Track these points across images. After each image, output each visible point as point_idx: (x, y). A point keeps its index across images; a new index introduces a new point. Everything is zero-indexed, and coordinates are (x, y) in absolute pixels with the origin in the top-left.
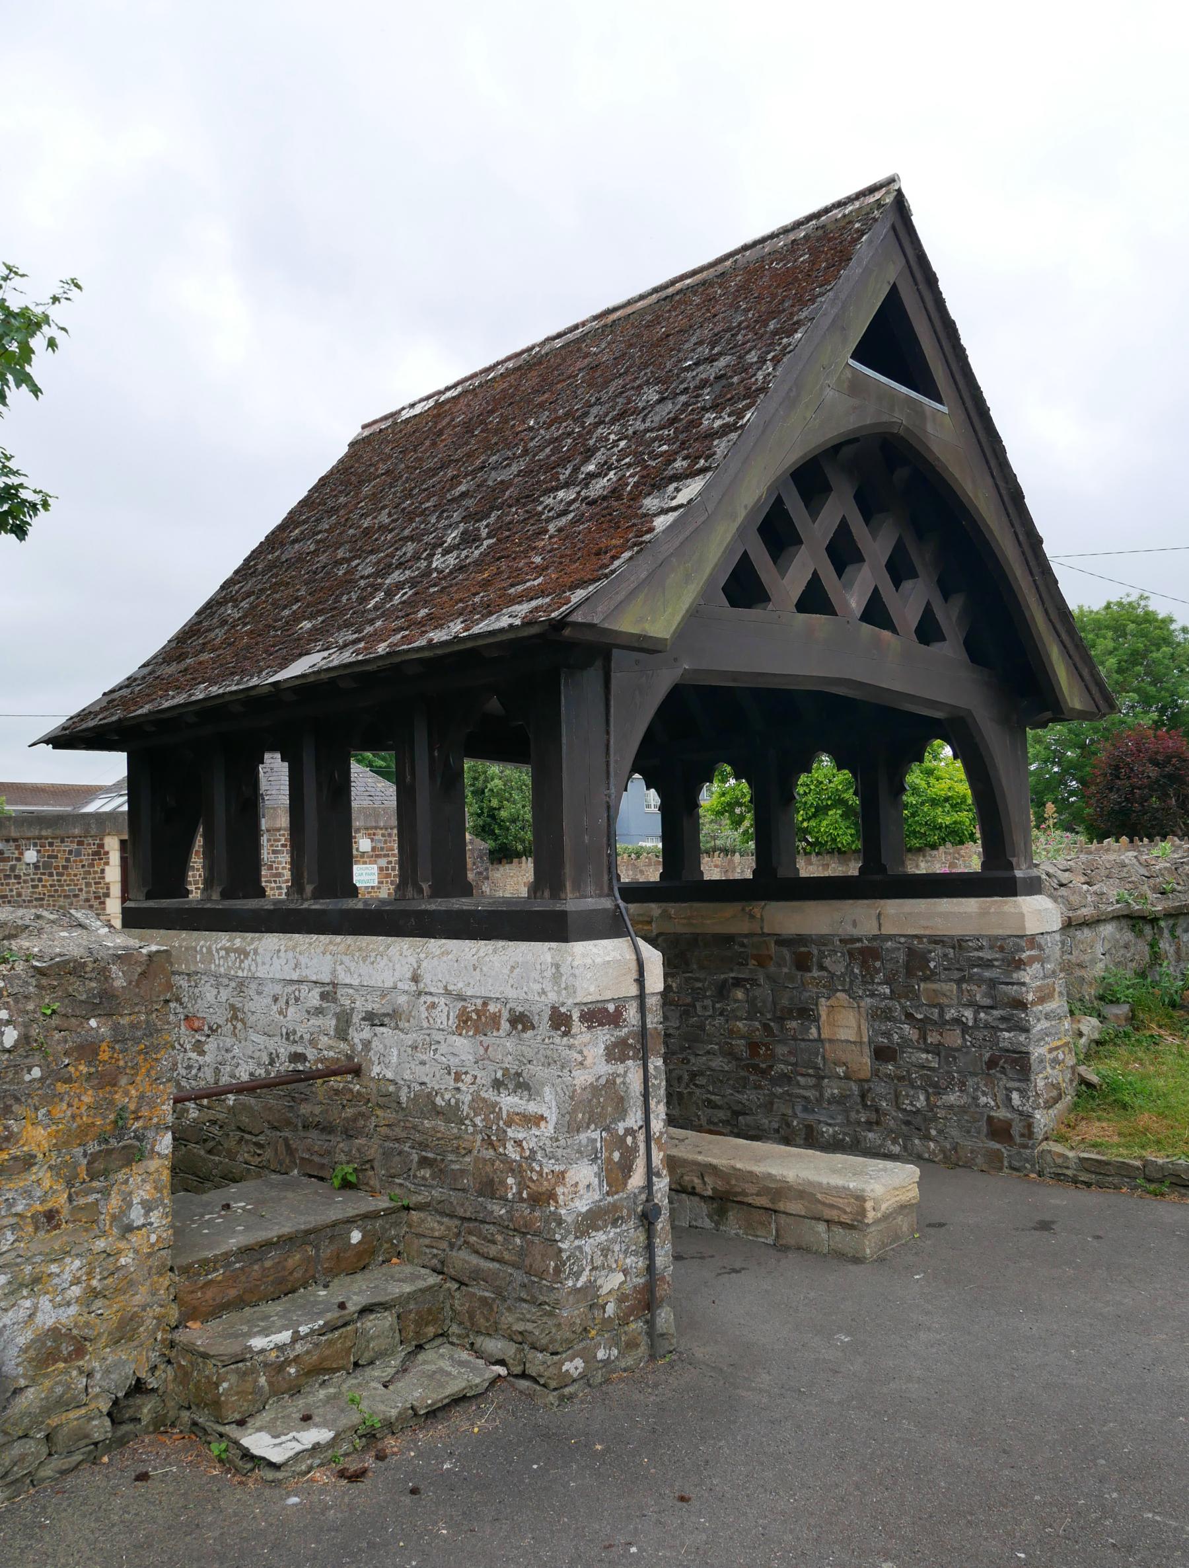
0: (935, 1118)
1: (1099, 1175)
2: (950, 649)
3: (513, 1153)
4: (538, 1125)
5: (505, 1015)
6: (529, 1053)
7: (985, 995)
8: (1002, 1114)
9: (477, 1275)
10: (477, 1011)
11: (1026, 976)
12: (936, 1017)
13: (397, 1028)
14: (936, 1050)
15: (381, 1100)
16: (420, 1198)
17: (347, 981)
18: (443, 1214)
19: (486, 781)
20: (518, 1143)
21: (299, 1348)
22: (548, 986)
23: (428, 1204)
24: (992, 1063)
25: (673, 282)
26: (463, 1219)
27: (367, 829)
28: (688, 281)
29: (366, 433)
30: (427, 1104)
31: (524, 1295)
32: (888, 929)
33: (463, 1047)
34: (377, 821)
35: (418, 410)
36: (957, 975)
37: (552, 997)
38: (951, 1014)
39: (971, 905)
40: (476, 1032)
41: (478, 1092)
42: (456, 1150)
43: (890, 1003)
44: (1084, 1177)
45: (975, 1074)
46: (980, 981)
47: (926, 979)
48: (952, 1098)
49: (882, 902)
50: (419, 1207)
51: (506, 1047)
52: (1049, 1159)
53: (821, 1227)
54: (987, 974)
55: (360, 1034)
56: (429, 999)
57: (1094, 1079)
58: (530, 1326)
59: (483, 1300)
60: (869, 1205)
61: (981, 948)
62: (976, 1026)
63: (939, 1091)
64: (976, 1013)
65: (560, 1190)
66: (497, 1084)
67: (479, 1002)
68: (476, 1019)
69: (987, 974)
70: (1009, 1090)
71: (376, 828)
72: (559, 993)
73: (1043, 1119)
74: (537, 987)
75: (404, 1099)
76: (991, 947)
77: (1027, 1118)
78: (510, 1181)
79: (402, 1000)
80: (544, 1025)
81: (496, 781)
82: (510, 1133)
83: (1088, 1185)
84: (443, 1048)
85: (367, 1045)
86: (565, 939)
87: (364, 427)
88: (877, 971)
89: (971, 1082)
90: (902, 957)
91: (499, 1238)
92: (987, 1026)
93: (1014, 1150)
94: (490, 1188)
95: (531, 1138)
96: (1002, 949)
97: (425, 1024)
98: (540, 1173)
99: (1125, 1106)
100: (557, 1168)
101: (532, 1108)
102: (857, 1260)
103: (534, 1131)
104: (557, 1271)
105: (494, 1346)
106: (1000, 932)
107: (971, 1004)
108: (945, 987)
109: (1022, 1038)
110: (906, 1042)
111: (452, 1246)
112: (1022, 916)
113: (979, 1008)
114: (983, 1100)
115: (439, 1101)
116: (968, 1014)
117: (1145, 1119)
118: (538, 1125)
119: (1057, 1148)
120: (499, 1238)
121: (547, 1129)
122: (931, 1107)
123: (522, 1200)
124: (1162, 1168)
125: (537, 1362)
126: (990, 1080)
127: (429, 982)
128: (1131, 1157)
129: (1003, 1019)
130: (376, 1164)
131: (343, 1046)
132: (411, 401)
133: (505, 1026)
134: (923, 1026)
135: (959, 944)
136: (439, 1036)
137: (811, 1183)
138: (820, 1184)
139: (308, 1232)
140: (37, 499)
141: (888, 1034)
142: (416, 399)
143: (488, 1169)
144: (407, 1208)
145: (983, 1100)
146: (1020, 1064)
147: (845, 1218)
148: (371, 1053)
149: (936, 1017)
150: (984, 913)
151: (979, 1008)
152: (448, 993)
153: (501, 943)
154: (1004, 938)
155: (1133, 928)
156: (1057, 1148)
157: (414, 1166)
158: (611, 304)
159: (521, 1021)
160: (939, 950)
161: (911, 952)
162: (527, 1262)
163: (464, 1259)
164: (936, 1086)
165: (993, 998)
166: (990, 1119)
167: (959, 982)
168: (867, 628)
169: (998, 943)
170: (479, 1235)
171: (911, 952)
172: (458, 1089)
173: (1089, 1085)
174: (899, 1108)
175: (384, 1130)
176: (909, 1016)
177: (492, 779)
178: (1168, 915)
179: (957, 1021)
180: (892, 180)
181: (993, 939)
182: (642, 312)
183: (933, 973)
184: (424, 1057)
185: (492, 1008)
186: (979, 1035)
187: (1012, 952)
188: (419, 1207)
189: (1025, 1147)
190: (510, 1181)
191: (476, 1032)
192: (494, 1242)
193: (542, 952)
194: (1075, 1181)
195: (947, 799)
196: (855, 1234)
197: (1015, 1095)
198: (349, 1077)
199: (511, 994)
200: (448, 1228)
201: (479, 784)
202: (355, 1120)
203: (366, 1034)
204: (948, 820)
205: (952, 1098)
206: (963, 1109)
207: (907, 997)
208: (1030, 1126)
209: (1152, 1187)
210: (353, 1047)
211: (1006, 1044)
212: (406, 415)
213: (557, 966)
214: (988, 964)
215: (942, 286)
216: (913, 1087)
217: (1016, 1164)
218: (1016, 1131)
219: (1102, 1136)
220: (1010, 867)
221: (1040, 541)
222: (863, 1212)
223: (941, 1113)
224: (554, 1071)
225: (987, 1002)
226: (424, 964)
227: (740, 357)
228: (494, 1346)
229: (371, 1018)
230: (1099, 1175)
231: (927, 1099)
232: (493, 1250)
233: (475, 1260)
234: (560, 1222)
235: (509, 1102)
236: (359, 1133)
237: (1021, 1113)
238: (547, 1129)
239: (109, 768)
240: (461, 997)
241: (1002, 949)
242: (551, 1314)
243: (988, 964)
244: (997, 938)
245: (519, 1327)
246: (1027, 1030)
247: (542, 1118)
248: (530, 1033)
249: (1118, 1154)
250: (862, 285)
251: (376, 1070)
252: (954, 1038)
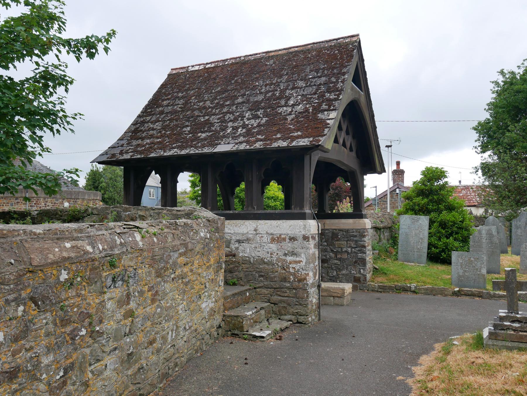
0: (339, 278)
1: (383, 289)
2: (354, 154)
3: (291, 270)
4: (300, 263)
5: (287, 237)
6: (296, 246)
7: (354, 244)
8: (358, 275)
9: (281, 301)
10: (278, 238)
11: (366, 239)
12: (340, 251)
13: (248, 243)
14: (340, 259)
15: (243, 262)
16: (260, 285)
17: (229, 232)
18: (267, 288)
19: (99, 183)
20: (294, 268)
21: (253, 316)
22: (301, 230)
23: (262, 286)
24: (356, 262)
25: (291, 48)
26: (275, 288)
27: (67, 199)
28: (296, 49)
29: (174, 72)
30: (262, 261)
31: (297, 303)
32: (326, 227)
33: (274, 247)
34: (71, 196)
35: (197, 68)
36: (346, 239)
37: (303, 233)
38: (344, 250)
39: (351, 221)
40: (278, 242)
41: (279, 257)
42: (272, 272)
43: (327, 247)
44: (380, 290)
45: (350, 265)
46: (353, 241)
47: (337, 240)
48: (344, 272)
49: (325, 220)
50: (259, 287)
51: (288, 246)
52: (370, 286)
53: (332, 298)
54: (355, 239)
55: (233, 246)
56: (260, 235)
57: (377, 267)
58: (299, 311)
59: (284, 307)
60: (345, 291)
61: (353, 232)
62: (351, 252)
63: (340, 270)
64: (352, 249)
65: (307, 277)
66: (285, 255)
67: (278, 235)
68: (277, 239)
69: (355, 239)
70: (360, 269)
71: (71, 199)
72: (305, 232)
73: (368, 276)
74: (299, 231)
75: (252, 261)
76: (356, 232)
77: (365, 276)
78: (291, 277)
79: (251, 236)
80: (300, 240)
81: (104, 184)
82: (290, 266)
83: (381, 292)
84: (266, 247)
85: (237, 248)
86: (305, 219)
87: (172, 69)
88: (323, 239)
89: (349, 267)
90: (330, 235)
91: (288, 291)
92: (355, 252)
93: (361, 285)
94: (285, 279)
95: (297, 267)
96: (359, 232)
97: (259, 242)
98: (301, 274)
99: (386, 274)
100: (306, 272)
101: (298, 259)
102: (342, 305)
103: (298, 264)
104: (307, 296)
105: (288, 317)
106: (359, 228)
107: (350, 247)
108: (343, 242)
109: (364, 255)
110: (331, 258)
111: (271, 295)
112: (365, 224)
113: (352, 248)
114: (353, 272)
115: (265, 260)
116: (349, 249)
117: (391, 276)
118: (300, 263)
119: (372, 283)
120: (288, 291)
121: (303, 264)
122: (338, 275)
123: (295, 281)
124: (400, 286)
125: (301, 319)
126: (355, 267)
127: (260, 230)
128: (392, 284)
129: (359, 250)
130: (243, 279)
131: (229, 249)
132: (192, 65)
133: (288, 240)
134: (336, 253)
135: (347, 231)
136: (265, 244)
137: (329, 287)
138: (332, 287)
139: (241, 292)
140: (69, 80)
141: (325, 256)
142: (195, 64)
143: (284, 275)
144: (255, 288)
145: (353, 272)
146: (363, 262)
147: (339, 295)
148: (239, 250)
149: (340, 251)
150: (355, 223)
151: (352, 248)
152: (267, 233)
153: (284, 221)
154: (360, 229)
155: (376, 231)
156: (372, 283)
157: (257, 277)
158: (270, 50)
159: (293, 239)
160: (341, 233)
161: (333, 233)
162: (298, 296)
163: (275, 298)
164: (339, 269)
165: (357, 245)
166: (354, 277)
167: (347, 241)
168: (343, 147)
169: (358, 231)
170: (281, 291)
171: (333, 233)
172: (272, 257)
173: (376, 269)
174: (328, 276)
175: (245, 270)
176: (332, 251)
177: (102, 183)
178: (383, 228)
179: (346, 251)
180: (358, 35)
181: (357, 230)
182: (282, 55)
183: (339, 239)
184: (260, 250)
185: (283, 236)
186: (352, 255)
187: (362, 233)
188: (259, 287)
189: (364, 283)
190: (291, 277)
191: (278, 242)
192: (286, 293)
193: (300, 222)
194: (377, 291)
195: (272, 198)
196: (342, 299)
197: (362, 270)
198: (231, 257)
199: (289, 232)
200: (270, 291)
201: (96, 184)
202: (234, 268)
203: (237, 245)
204: (273, 204)
205: (344, 272)
206: (347, 275)
207: (332, 246)
208: (366, 278)
209: (398, 291)
210: (232, 249)
211: (360, 257)
212: (191, 69)
213: (305, 225)
214: (356, 236)
215: (365, 62)
216: (332, 270)
217: (361, 288)
218: (361, 280)
219: (381, 280)
220: (361, 211)
221: (376, 128)
222: (344, 293)
223: (341, 276)
224: (304, 250)
225: (355, 246)
226: (259, 226)
227: (329, 79)
228: (288, 317)
229: (239, 241)
230: (383, 289)
231: (337, 273)
232: (286, 295)
233: (280, 298)
234: (308, 285)
235: (289, 259)
236: (235, 271)
237: (363, 275)
238: (303, 264)
239: (119, 171)
240: (272, 234)
241: (359, 232)
242: (305, 307)
243: (356, 236)
244: (358, 229)
245: (297, 311)
246: (365, 253)
247: (301, 261)
248: (296, 242)
249: (387, 284)
250: (342, 59)
251: (241, 255)
252: (345, 256)
